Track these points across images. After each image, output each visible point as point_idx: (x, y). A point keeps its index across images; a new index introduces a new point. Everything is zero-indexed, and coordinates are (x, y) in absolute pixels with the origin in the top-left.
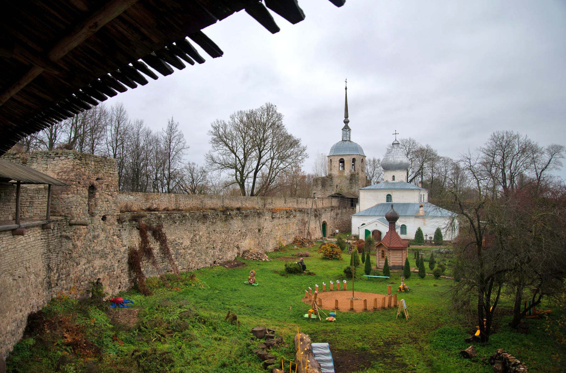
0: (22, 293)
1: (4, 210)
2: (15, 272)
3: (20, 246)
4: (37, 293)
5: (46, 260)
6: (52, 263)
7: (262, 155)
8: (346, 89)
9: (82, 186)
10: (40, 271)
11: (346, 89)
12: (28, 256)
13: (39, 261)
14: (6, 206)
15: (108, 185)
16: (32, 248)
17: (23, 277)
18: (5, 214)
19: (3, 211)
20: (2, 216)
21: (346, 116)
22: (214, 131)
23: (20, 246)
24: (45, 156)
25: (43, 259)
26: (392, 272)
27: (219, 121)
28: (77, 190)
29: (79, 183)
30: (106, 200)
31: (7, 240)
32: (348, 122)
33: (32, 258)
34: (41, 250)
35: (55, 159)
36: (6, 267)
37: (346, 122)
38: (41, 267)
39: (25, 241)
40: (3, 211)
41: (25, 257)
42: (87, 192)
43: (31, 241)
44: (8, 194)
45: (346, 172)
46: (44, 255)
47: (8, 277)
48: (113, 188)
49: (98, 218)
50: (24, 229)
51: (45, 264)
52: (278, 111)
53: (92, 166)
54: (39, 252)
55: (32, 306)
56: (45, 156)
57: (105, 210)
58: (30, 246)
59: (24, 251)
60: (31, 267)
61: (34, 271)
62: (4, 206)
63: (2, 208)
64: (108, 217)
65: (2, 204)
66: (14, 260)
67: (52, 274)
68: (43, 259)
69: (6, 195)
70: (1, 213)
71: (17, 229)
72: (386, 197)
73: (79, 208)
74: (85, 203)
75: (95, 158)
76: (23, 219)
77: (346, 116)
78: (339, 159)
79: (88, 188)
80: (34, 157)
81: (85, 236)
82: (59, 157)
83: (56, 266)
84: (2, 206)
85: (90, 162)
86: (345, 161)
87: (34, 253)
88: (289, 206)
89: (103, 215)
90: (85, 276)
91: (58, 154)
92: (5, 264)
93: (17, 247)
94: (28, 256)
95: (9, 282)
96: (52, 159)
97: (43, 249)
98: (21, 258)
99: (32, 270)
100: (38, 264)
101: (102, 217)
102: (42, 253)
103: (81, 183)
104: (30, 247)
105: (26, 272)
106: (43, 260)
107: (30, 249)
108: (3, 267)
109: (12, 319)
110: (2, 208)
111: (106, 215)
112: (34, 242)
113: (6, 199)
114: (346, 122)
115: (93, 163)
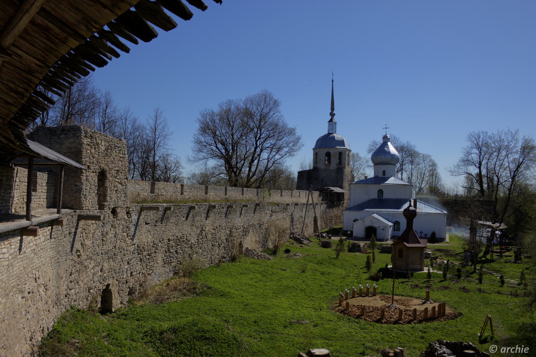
0: (32, 314)
1: (6, 200)
2: (25, 286)
3: (29, 250)
4: (47, 311)
5: (55, 265)
6: (61, 268)
7: (155, 161)
8: (333, 81)
9: (91, 171)
10: (50, 280)
11: (333, 81)
12: (38, 262)
13: (49, 268)
14: (7, 194)
15: (118, 171)
16: (41, 251)
17: (32, 292)
18: (6, 206)
19: (4, 201)
20: (3, 208)
21: (333, 109)
22: (201, 119)
23: (29, 250)
24: (48, 133)
25: (52, 264)
26: (403, 270)
27: (207, 109)
28: (87, 176)
29: (89, 167)
30: (116, 189)
31: (15, 243)
32: (334, 115)
33: (42, 265)
34: (51, 253)
35: (60, 137)
36: (14, 282)
37: (332, 115)
38: (50, 275)
39: (35, 242)
40: (4, 201)
41: (34, 264)
42: (97, 179)
43: (41, 242)
44: (10, 179)
45: (332, 166)
46: (54, 259)
47: (17, 295)
48: (123, 174)
49: (107, 211)
50: (38, 227)
51: (55, 270)
52: (275, 98)
53: (102, 147)
54: (49, 256)
55: (42, 329)
56: (48, 133)
57: (115, 202)
58: (40, 249)
59: (34, 256)
60: (41, 277)
61: (43, 282)
62: (6, 195)
63: (3, 196)
64: (118, 210)
65: (2, 191)
66: (23, 271)
67: (61, 283)
68: (52, 264)
69: (8, 179)
70: (2, 204)
71: (28, 227)
72: (377, 192)
73: (88, 198)
74: (94, 192)
75: (106, 138)
76: (464, 240)
77: (333, 109)
78: (325, 152)
79: (98, 174)
80: (36, 134)
81: (93, 234)
82: (66, 134)
83: (65, 272)
84: (3, 195)
85: (100, 142)
86: (331, 155)
87: (43, 257)
88: (284, 200)
89: (113, 206)
90: (94, 282)
91: (64, 131)
92: (13, 278)
93: (27, 251)
94: (38, 262)
95: (18, 302)
96: (57, 137)
97: (52, 252)
98: (30, 267)
99: (41, 281)
100: (48, 272)
101: (111, 210)
102: (51, 257)
103: (90, 167)
104: (39, 251)
105: (35, 284)
106: (53, 266)
107: (39, 252)
108: (11, 282)
109: (21, 353)
110: (3, 196)
111: (116, 207)
112: (44, 244)
113: (8, 185)
114: (332, 115)
115: (103, 143)
